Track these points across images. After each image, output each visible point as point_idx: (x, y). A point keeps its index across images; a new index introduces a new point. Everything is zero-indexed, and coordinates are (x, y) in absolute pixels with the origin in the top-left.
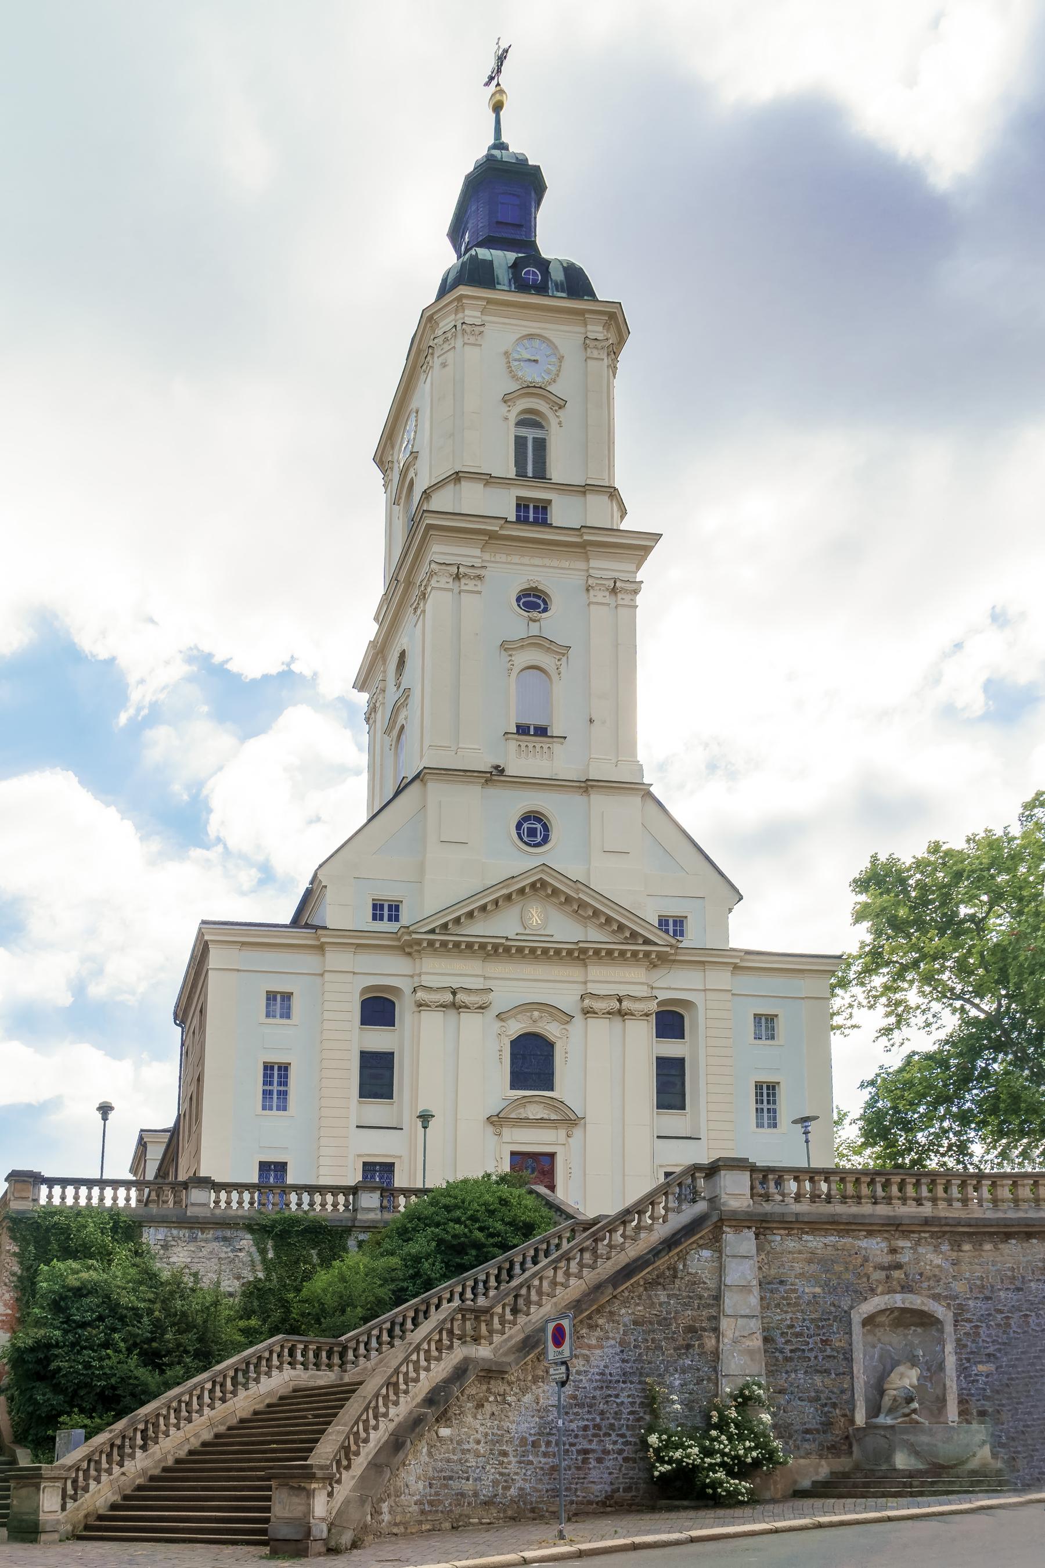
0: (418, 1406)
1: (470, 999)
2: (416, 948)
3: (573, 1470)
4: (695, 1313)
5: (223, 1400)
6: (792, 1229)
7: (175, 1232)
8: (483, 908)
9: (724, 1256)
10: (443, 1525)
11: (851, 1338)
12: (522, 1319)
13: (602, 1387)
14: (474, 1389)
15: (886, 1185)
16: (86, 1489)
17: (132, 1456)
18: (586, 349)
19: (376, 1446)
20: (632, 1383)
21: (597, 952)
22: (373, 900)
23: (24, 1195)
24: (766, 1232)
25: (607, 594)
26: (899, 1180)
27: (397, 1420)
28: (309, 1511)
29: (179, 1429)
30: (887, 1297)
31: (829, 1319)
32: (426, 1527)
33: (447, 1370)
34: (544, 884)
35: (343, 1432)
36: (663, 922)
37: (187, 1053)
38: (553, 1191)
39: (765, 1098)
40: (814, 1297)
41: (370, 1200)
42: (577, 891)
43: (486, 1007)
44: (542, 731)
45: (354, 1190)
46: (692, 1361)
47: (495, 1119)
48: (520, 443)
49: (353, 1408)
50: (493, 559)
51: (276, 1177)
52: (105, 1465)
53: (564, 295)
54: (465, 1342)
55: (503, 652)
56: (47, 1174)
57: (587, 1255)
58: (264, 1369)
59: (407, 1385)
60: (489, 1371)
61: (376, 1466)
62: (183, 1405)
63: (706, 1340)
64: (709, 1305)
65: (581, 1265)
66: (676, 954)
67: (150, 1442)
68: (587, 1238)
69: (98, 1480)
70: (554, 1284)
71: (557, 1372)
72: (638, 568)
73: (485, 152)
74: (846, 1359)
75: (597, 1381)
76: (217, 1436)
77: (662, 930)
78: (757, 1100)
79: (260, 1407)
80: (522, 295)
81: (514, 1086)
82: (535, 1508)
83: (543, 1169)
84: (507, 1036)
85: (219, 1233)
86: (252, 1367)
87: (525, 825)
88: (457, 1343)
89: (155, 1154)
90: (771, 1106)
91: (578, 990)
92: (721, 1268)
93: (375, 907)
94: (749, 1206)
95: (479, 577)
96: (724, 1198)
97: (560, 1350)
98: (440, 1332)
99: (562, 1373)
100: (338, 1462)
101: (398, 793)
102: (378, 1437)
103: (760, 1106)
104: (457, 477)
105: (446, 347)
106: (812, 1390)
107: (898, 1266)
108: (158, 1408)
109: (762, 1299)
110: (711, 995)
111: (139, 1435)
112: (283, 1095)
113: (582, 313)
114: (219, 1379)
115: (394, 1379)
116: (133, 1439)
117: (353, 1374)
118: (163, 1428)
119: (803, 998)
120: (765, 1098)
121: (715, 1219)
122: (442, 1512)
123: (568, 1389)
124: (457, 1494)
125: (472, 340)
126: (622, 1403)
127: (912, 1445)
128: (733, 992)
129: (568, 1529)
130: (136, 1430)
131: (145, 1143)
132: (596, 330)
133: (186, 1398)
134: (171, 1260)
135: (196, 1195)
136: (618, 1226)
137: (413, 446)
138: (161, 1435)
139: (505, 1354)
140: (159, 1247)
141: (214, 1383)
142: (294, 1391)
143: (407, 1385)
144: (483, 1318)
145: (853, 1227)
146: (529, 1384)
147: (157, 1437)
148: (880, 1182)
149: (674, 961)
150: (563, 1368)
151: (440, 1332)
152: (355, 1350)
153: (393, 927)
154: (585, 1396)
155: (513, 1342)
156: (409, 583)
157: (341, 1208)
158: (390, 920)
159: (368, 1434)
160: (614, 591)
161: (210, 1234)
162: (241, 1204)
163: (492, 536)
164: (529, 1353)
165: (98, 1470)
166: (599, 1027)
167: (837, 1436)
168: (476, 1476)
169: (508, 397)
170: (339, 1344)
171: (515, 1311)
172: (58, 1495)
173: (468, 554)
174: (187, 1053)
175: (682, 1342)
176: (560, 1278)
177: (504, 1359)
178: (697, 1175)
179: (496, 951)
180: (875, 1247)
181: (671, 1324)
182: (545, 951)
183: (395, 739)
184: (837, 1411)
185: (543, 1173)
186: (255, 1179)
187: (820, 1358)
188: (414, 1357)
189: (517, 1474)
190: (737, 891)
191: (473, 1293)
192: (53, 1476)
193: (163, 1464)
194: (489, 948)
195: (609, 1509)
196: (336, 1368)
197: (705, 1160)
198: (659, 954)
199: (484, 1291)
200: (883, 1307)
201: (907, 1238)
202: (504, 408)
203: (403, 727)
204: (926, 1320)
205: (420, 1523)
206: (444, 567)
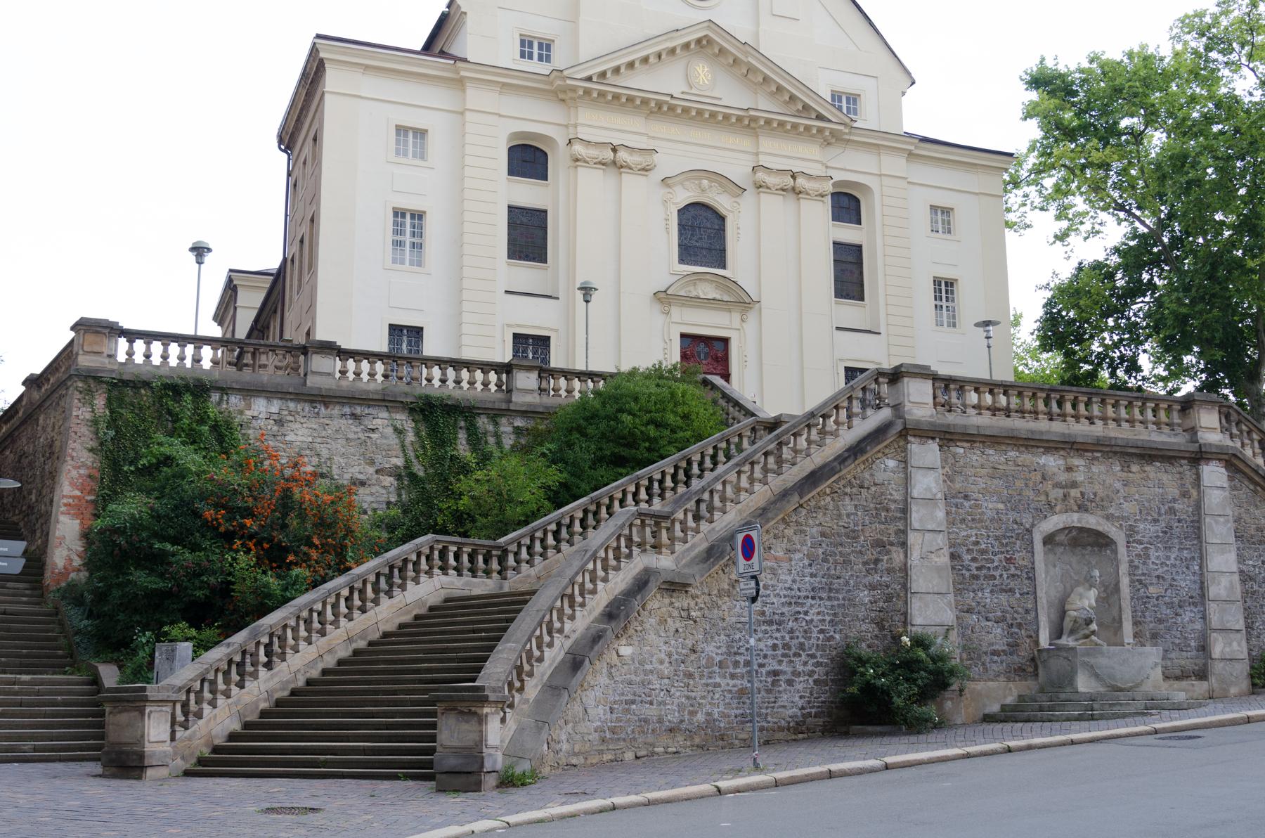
0: (596, 621)
2: (570, 94)
3: (763, 693)
5: (363, 610)
6: (974, 442)
7: (292, 405)
8: (645, 60)
10: (626, 755)
11: (1033, 556)
12: (704, 526)
13: (791, 603)
14: (656, 603)
16: (199, 715)
17: (255, 675)
19: (551, 665)
20: (821, 599)
22: (521, 35)
23: (96, 349)
27: (574, 637)
28: (481, 741)
29: (310, 643)
30: (1065, 516)
32: (608, 757)
33: (626, 580)
34: (710, 41)
35: (514, 650)
36: (836, 96)
39: (944, 295)
40: (998, 513)
41: (526, 381)
42: (746, 54)
45: (506, 369)
47: (663, 295)
49: (525, 623)
51: (409, 344)
52: (221, 686)
54: (644, 551)
56: (126, 325)
57: (771, 460)
58: (411, 574)
59: (584, 598)
60: (672, 583)
61: (554, 689)
62: (315, 615)
63: (894, 555)
65: (766, 470)
66: (850, 133)
67: (275, 659)
68: (771, 441)
69: (213, 704)
70: (738, 490)
74: (1029, 578)
76: (356, 652)
77: (834, 106)
79: (407, 618)
81: (682, 260)
82: (724, 735)
83: (716, 355)
85: (347, 410)
86: (396, 571)
88: (636, 550)
89: (250, 303)
90: (949, 304)
92: (907, 479)
93: (523, 43)
94: (932, 416)
96: (908, 406)
100: (511, 685)
102: (554, 655)
103: (939, 303)
107: (1074, 485)
108: (284, 618)
110: (886, 181)
111: (262, 650)
115: (569, 591)
116: (254, 655)
117: (514, 582)
118: (290, 641)
119: (977, 194)
120: (944, 295)
122: (624, 740)
123: (757, 606)
124: (640, 720)
126: (812, 620)
127: (1092, 667)
129: (764, 757)
130: (258, 644)
131: (235, 286)
133: (319, 606)
134: (287, 438)
135: (320, 363)
136: (803, 429)
138: (288, 651)
139: (688, 565)
141: (352, 589)
142: (447, 600)
143: (584, 598)
144: (663, 524)
145: (1032, 443)
146: (715, 599)
147: (284, 653)
150: (753, 583)
151: (618, 538)
152: (516, 554)
153: (544, 68)
155: (696, 551)
157: (493, 388)
159: (542, 652)
161: (336, 411)
162: (371, 376)
165: (213, 692)
166: (773, 205)
167: (1024, 657)
168: (660, 699)
170: (497, 548)
171: (697, 518)
172: (167, 721)
176: (744, 482)
177: (687, 571)
178: (881, 380)
180: (1052, 462)
182: (713, 115)
184: (1023, 632)
185: (716, 359)
186: (382, 345)
187: (1005, 576)
189: (703, 697)
190: (909, 74)
192: (160, 698)
193: (293, 686)
194: (653, 104)
195: (801, 736)
196: (495, 575)
197: (888, 364)
198: (833, 132)
199: (659, 492)
200: (1061, 526)
201: (1081, 456)
204: (1101, 541)
205: (601, 752)
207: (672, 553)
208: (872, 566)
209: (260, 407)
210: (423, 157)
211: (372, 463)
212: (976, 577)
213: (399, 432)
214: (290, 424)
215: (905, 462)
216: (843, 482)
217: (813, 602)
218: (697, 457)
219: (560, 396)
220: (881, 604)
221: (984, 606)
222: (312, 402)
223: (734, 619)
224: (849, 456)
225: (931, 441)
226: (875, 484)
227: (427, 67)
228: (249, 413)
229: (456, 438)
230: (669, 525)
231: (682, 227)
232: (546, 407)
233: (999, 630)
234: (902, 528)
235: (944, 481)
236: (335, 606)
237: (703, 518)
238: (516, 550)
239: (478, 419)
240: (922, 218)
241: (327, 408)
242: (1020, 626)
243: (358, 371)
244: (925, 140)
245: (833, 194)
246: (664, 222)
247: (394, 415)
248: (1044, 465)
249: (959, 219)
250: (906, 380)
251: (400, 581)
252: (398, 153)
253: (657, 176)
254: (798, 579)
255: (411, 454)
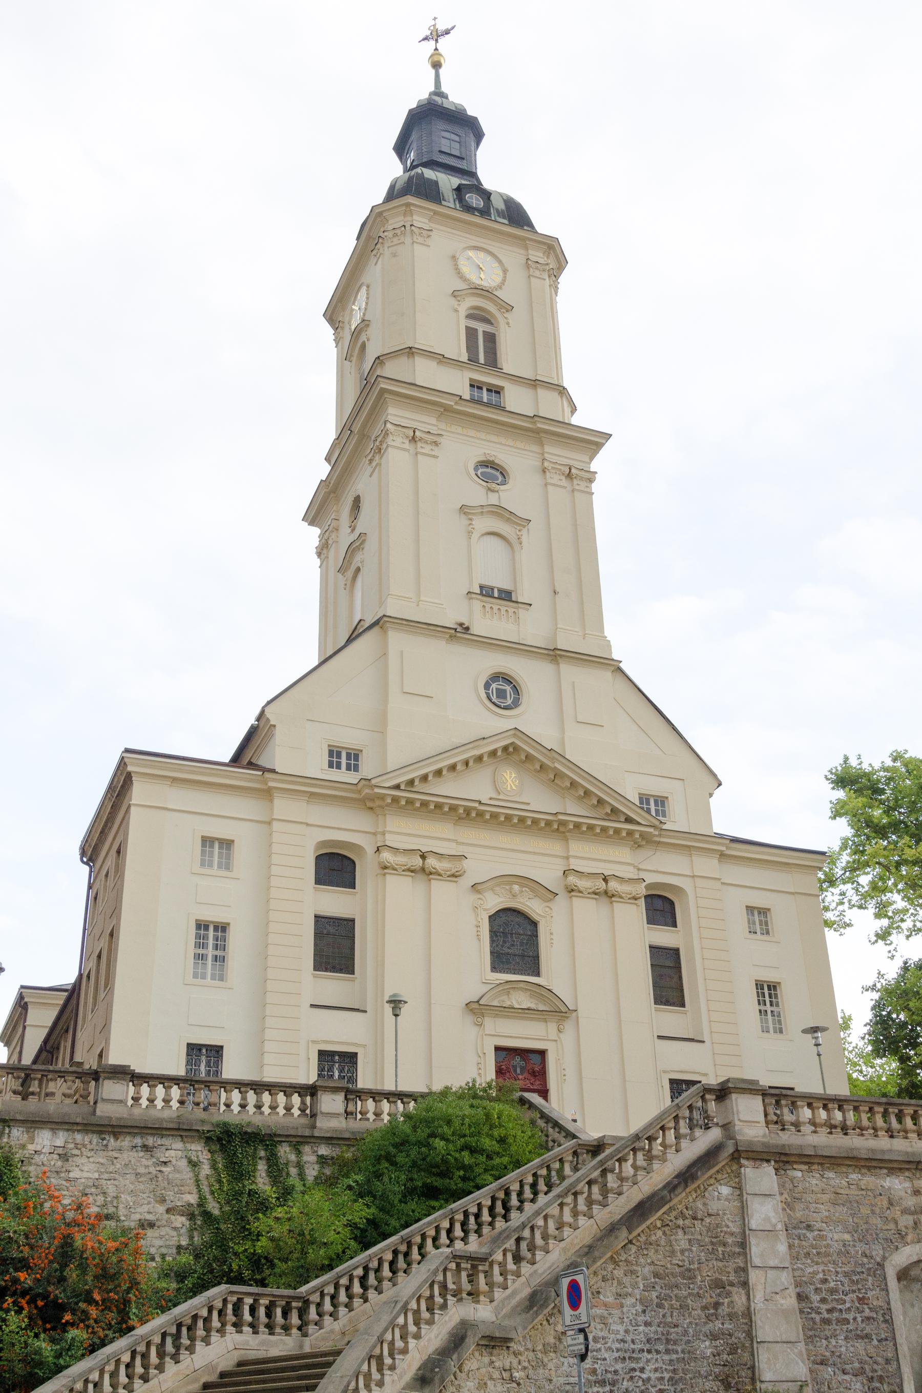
1: (441, 865)
2: (378, 803)
4: (720, 1264)
5: (145, 1378)
6: (813, 1163)
7: (79, 1137)
8: (453, 768)
9: (744, 1194)
11: (888, 1295)
12: (526, 1268)
13: (624, 1358)
15: (900, 1117)
18: (528, 268)
20: (658, 1352)
21: (577, 826)
22: (329, 746)
24: (785, 1168)
25: (563, 478)
26: (912, 1112)
31: (863, 1273)
33: (440, 1337)
34: (517, 749)
36: (644, 799)
37: (96, 898)
38: (547, 1100)
39: (767, 999)
40: (844, 1245)
42: (553, 760)
43: (460, 876)
44: (506, 596)
45: (311, 1091)
46: (723, 1324)
47: (475, 1006)
48: (471, 334)
50: (448, 429)
51: (208, 1064)
53: (506, 222)
54: (460, 1300)
55: (463, 516)
57: (595, 1189)
58: (200, 1332)
59: (394, 1359)
60: (491, 1338)
63: (736, 1298)
64: (735, 1253)
65: (590, 1202)
66: (660, 835)
68: (595, 1168)
71: (575, 1342)
72: (592, 459)
73: (426, 96)
74: (886, 1321)
75: (618, 1350)
77: (642, 808)
78: (759, 1001)
80: (466, 214)
81: (494, 969)
84: (485, 910)
85: (138, 1141)
87: (494, 686)
88: (451, 1300)
91: (560, 866)
92: (743, 1208)
93: (331, 753)
94: (764, 1136)
95: (436, 443)
96: (738, 1126)
97: (576, 1313)
98: (431, 1286)
99: (580, 1344)
101: (350, 641)
103: (763, 1008)
104: (410, 351)
105: (396, 240)
106: (855, 1359)
109: (790, 1247)
112: (220, 960)
113: (523, 239)
114: (141, 1348)
115: (377, 1351)
117: (316, 1339)
119: (792, 893)
121: (731, 1149)
125: (420, 240)
126: (649, 1379)
128: (723, 881)
131: (26, 1003)
132: (537, 255)
133: (95, 1376)
134: (72, 1175)
135: (111, 1089)
136: (628, 1153)
137: (364, 314)
139: (509, 1316)
140: (56, 1157)
142: (240, 1364)
143: (394, 1359)
145: (874, 1164)
148: (893, 1113)
149: (659, 842)
151: (431, 1286)
152: (319, 1305)
154: (606, 1370)
155: (518, 1298)
156: (364, 436)
157: (296, 1112)
158: (348, 768)
160: (569, 476)
161: (126, 1142)
163: (447, 409)
164: (537, 1314)
166: (585, 909)
169: (456, 293)
170: (298, 1298)
171: (517, 1259)
173: (424, 421)
174: (96, 898)
175: (709, 1300)
176: (567, 1217)
178: (708, 1096)
179: (468, 814)
181: (695, 1277)
183: (349, 583)
186: (180, 1070)
187: (859, 1319)
188: (401, 1320)
190: (715, 776)
191: (463, 1230)
194: (461, 811)
196: (294, 1331)
198: (643, 835)
199: (476, 1227)
200: (915, 1259)
202: (453, 302)
203: (358, 570)
206: (400, 429)
207: (491, 1301)
208: (712, 1311)
209: (45, 1140)
210: (228, 867)
211: (163, 1200)
212: (827, 1322)
213: (194, 1164)
214: (75, 1159)
215: (739, 1188)
216: (674, 1213)
217: (649, 1356)
218: (515, 1187)
219: (368, 1119)
220: (725, 1357)
221: (840, 1356)
222: (100, 1133)
223: (562, 1380)
224: (679, 1183)
225: (765, 1165)
226: (710, 1215)
227: (236, 778)
228: (31, 1147)
229: (255, 1170)
230: (486, 1268)
231: (493, 934)
232: (353, 1133)
233: (858, 1386)
234: (742, 1265)
235: (784, 1209)
236: (114, 1375)
237: (523, 1259)
238: (318, 1300)
239: (279, 1148)
240: (739, 920)
241: (116, 1139)
242: (881, 1379)
243: (152, 1097)
244: (735, 840)
245: (646, 897)
246: (475, 929)
247: (188, 1146)
248: (890, 1188)
249: (777, 919)
250: (734, 1096)
251: (188, 1342)
252: (203, 864)
253: (466, 882)
254: (631, 1328)
255: (206, 1189)
